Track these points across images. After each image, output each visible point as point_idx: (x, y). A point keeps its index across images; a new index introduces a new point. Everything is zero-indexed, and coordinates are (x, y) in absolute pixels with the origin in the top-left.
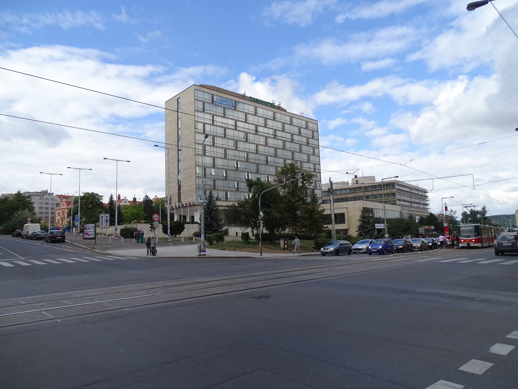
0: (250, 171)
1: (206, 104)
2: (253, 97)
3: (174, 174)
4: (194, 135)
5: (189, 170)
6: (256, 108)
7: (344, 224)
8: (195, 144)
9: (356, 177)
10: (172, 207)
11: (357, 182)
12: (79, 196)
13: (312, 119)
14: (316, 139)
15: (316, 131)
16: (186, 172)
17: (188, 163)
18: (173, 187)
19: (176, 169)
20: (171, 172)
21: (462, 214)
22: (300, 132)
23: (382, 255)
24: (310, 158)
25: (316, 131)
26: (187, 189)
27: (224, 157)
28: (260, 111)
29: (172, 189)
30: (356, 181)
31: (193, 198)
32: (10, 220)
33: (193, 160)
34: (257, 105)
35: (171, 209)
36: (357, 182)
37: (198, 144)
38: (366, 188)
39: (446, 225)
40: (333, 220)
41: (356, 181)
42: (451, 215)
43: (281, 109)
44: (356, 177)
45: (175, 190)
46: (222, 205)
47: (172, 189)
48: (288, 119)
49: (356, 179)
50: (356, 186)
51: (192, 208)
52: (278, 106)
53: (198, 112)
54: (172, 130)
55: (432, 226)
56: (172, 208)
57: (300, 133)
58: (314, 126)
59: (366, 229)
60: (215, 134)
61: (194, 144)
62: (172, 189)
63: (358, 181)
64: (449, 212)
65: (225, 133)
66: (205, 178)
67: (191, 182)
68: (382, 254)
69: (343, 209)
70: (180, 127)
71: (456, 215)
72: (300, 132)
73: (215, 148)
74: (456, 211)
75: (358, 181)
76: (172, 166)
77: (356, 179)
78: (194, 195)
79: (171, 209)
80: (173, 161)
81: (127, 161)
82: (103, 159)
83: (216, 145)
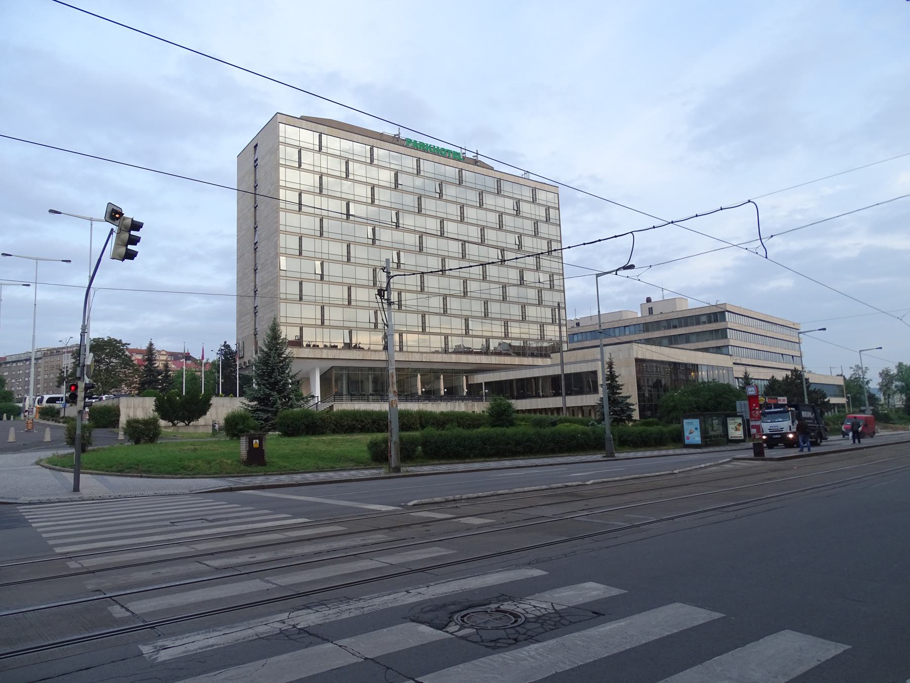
0: (526, 302)
6: (418, 160)
7: (596, 395)
9: (649, 300)
11: (651, 310)
12: (81, 345)
13: (545, 183)
15: (554, 208)
21: (881, 374)
23: (795, 447)
25: (554, 208)
28: (427, 167)
32: (394, 392)
34: (420, 154)
36: (651, 310)
38: (670, 323)
39: (784, 400)
40: (393, 388)
42: (858, 376)
43: (479, 164)
44: (649, 300)
46: (372, 359)
47: (246, 328)
48: (491, 184)
49: (650, 305)
50: (650, 319)
52: (474, 158)
53: (355, 184)
55: (779, 398)
56: (244, 365)
59: (618, 407)
63: (652, 308)
64: (853, 369)
65: (442, 227)
68: (795, 446)
69: (593, 363)
71: (868, 376)
74: (866, 368)
75: (652, 308)
77: (650, 305)
80: (247, 270)
81: (819, 330)
82: (827, 328)
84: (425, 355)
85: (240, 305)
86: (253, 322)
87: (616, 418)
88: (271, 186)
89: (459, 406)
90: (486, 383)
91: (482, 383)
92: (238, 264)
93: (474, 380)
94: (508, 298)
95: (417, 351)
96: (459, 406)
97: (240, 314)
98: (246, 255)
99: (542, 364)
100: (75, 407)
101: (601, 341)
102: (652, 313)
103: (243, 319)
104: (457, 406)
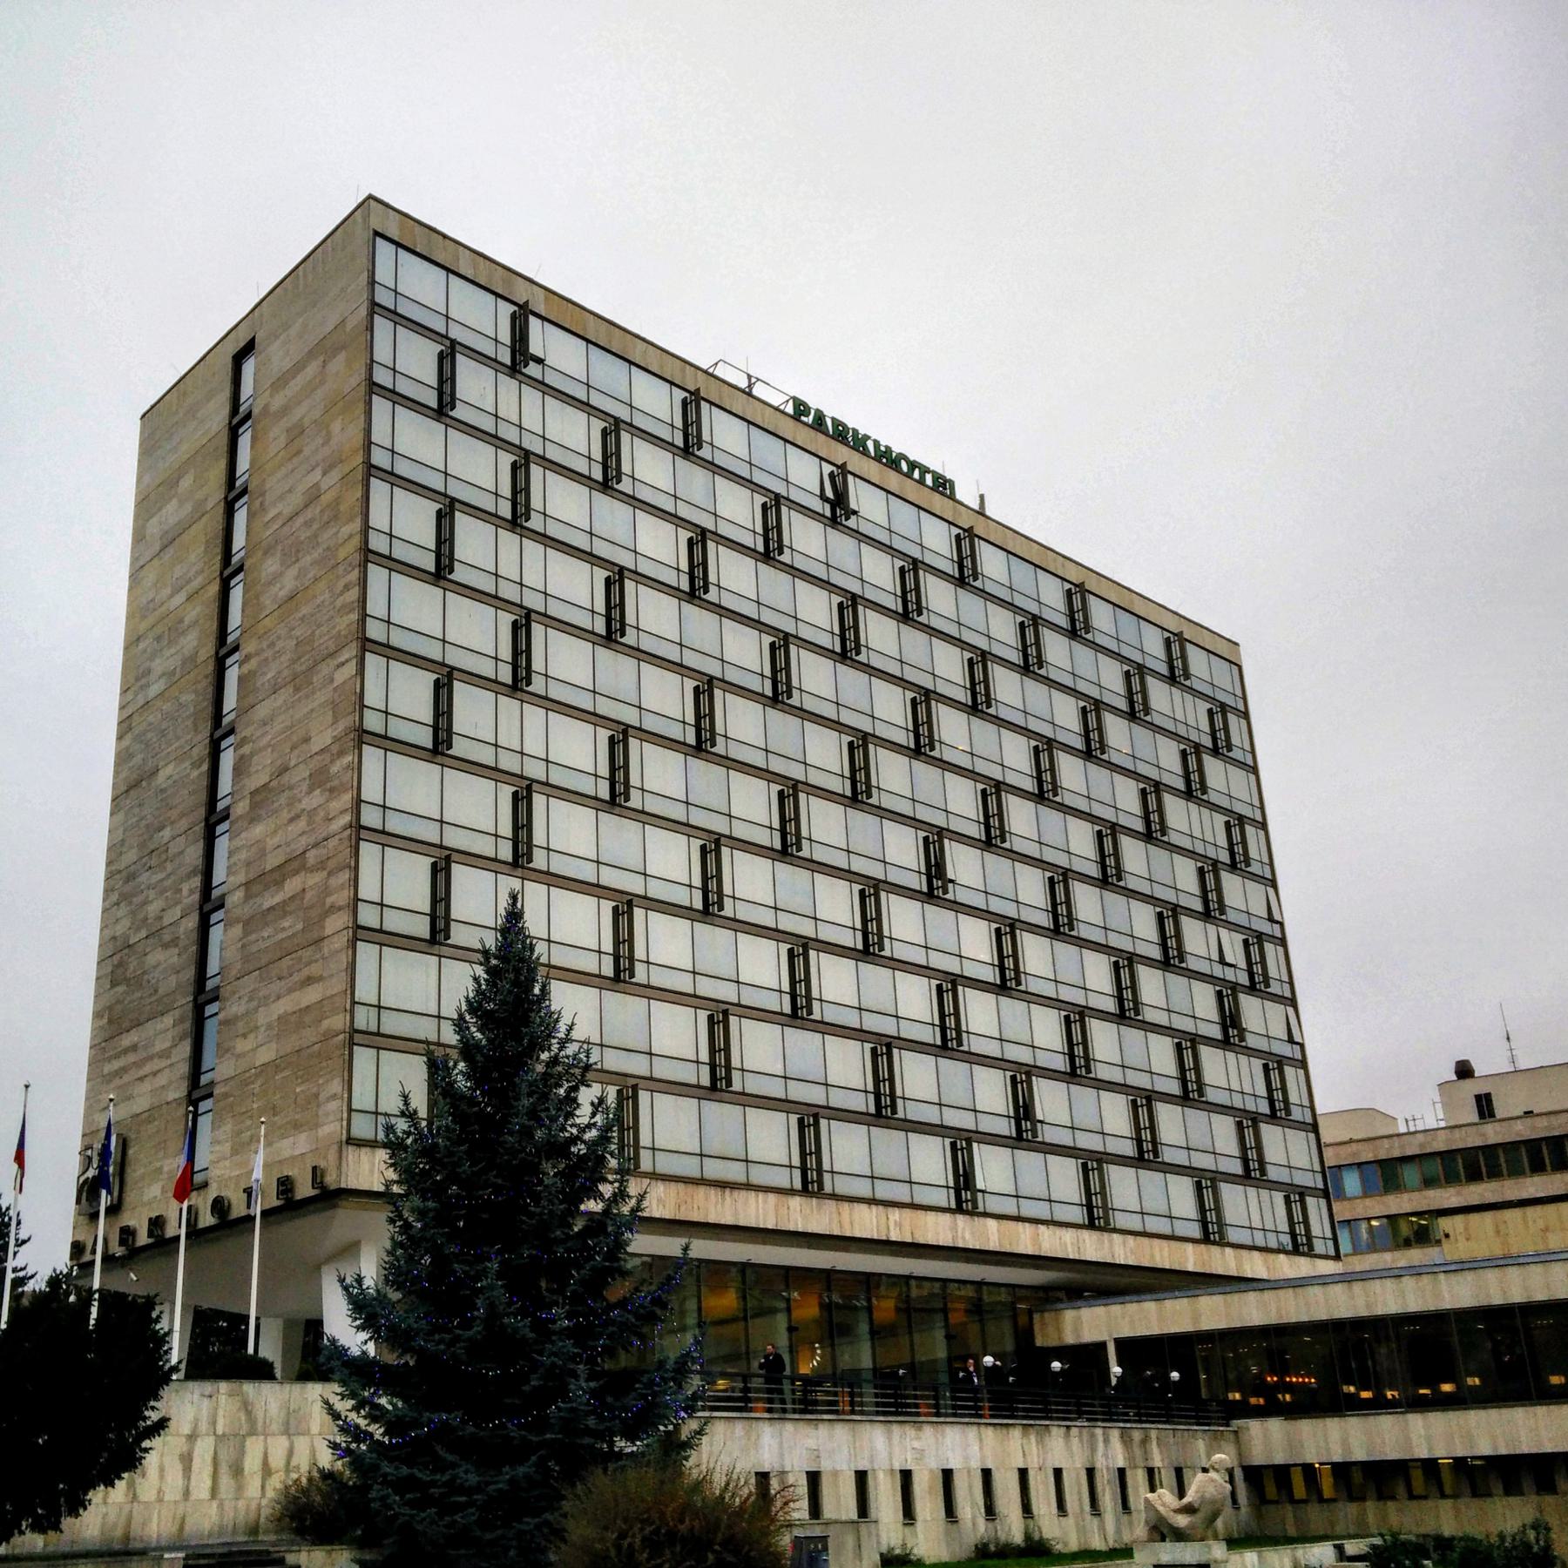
1: (464, 524)
2: (814, 403)
3: (166, 946)
4: (354, 575)
5: (292, 885)
8: (364, 650)
9: (1464, 1071)
10: (127, 1234)
11: (1485, 1105)
14: (1240, 764)
16: (267, 905)
17: (292, 820)
18: (151, 1058)
19: (191, 892)
20: (143, 934)
22: (1023, 1111)
24: (1103, 1186)
26: (266, 1055)
27: (608, 970)
29: (141, 1073)
30: (1478, 1098)
31: (317, 1126)
33: (331, 790)
35: (118, 1251)
36: (1485, 1105)
37: (388, 744)
41: (1478, 1098)
44: (1464, 1071)
45: (162, 1080)
46: (712, 1219)
47: (141, 1079)
49: (1470, 1088)
51: (301, 1229)
54: (180, 598)
56: (122, 1242)
57: (1026, 1125)
58: (1222, 676)
60: (535, 770)
61: (351, 651)
62: (141, 1079)
63: (1488, 1096)
66: (445, 950)
67: (309, 981)
70: (242, 553)
72: (1023, 1111)
73: (535, 715)
75: (1488, 1096)
76: (160, 876)
78: (334, 1097)
79: (118, 1251)
83: (539, 860)
84: (895, 1215)
85: (114, 984)
86: (186, 1048)
87: (445, 1423)
88: (324, 474)
89: (1345, 1442)
90: (1120, 1343)
91: (1102, 1346)
92: (120, 816)
93: (1059, 1330)
94: (736, 1076)
95: (866, 1196)
96: (1345, 1442)
97: (110, 1021)
98: (162, 774)
99: (1265, 1277)
100: (178, 1452)
101: (686, 1249)
102: (1492, 1115)
103: (127, 1040)
104: (1100, 1439)
